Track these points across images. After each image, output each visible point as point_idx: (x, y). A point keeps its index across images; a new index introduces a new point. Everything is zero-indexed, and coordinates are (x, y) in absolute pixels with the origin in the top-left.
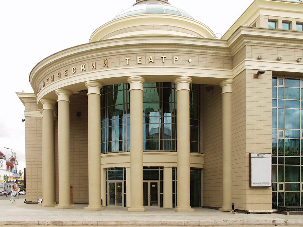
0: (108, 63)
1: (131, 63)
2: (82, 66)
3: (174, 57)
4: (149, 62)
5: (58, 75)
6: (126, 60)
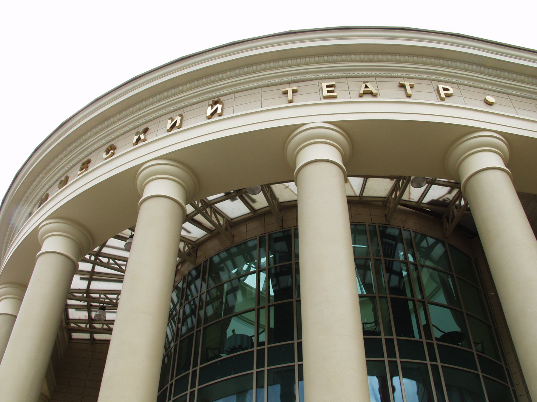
3: (441, 87)
6: (285, 95)
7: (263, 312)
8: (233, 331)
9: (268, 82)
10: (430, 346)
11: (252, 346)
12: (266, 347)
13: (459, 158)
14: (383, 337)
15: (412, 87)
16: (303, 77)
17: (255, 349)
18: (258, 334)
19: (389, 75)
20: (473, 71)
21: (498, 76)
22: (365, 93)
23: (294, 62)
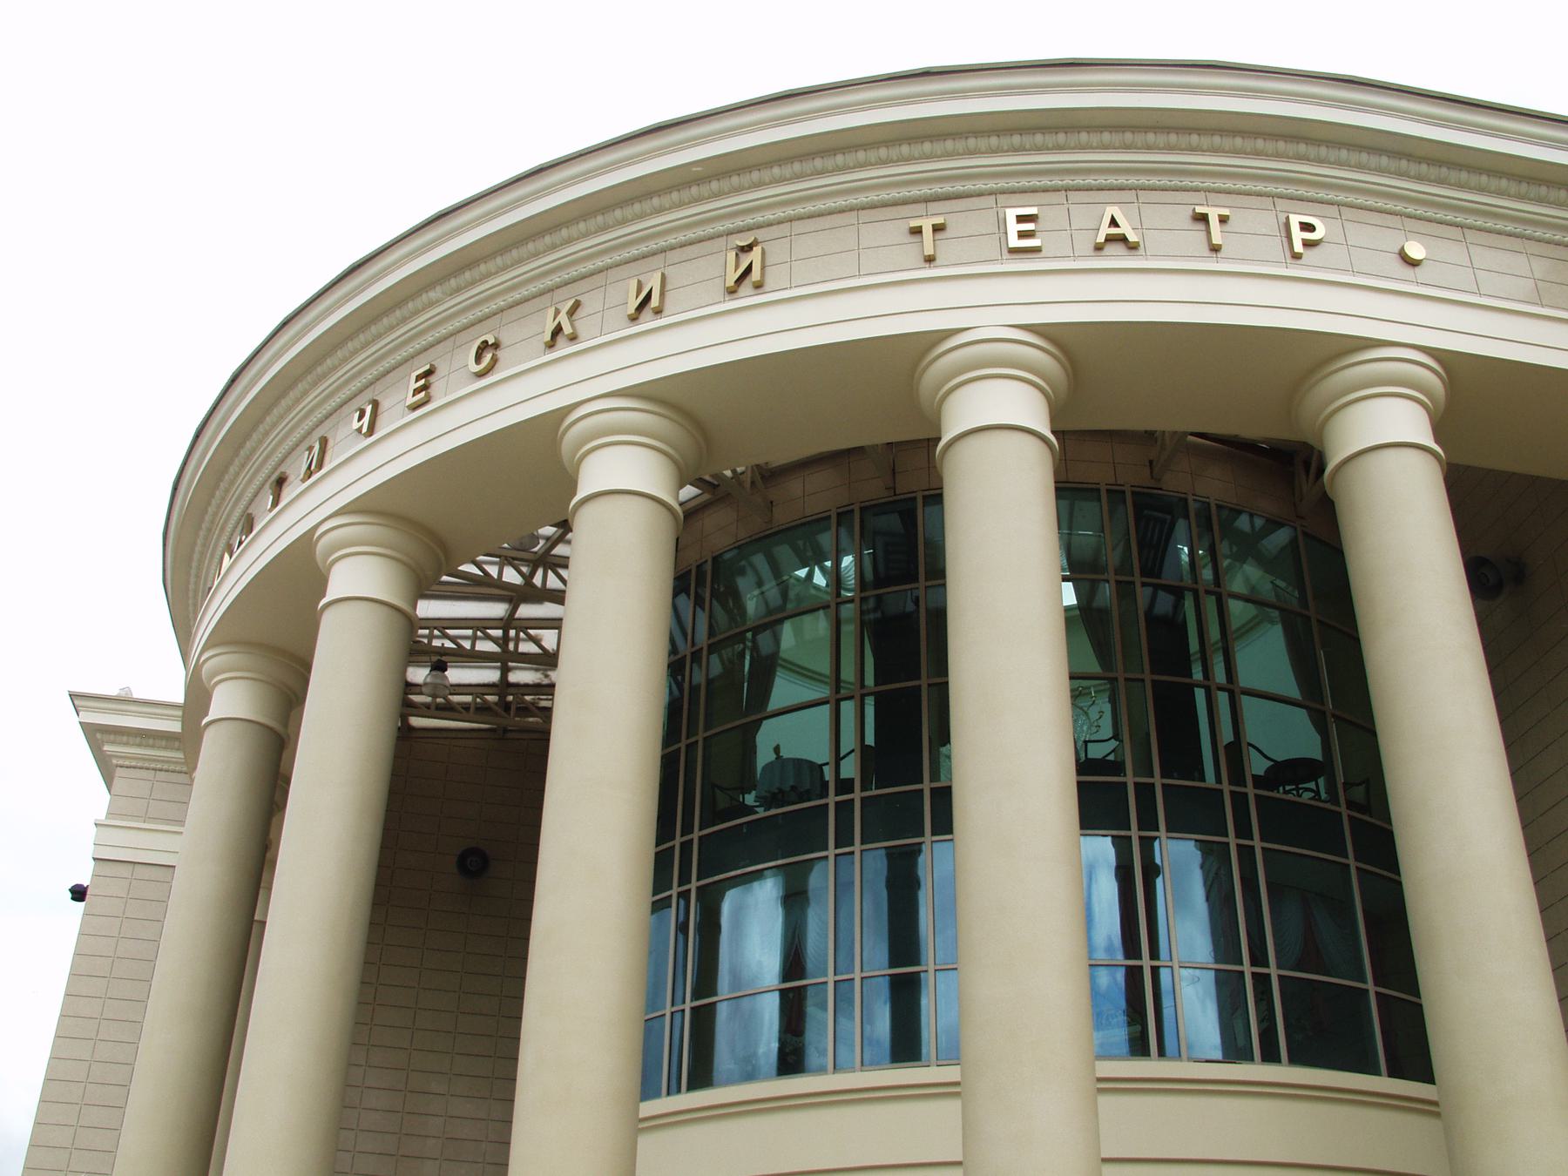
0: (763, 267)
1: (947, 249)
2: (551, 311)
3: (1295, 220)
4: (1101, 239)
5: (360, 418)
6: (916, 238)
7: (848, 708)
8: (777, 749)
9: (873, 197)
10: (1240, 801)
11: (825, 794)
12: (857, 795)
13: (1332, 401)
14: (1130, 779)
15: (1223, 220)
16: (959, 187)
17: (832, 799)
18: (838, 759)
19: (1173, 183)
20: (1380, 171)
21: (1440, 182)
22: (1110, 239)
23: (938, 147)
